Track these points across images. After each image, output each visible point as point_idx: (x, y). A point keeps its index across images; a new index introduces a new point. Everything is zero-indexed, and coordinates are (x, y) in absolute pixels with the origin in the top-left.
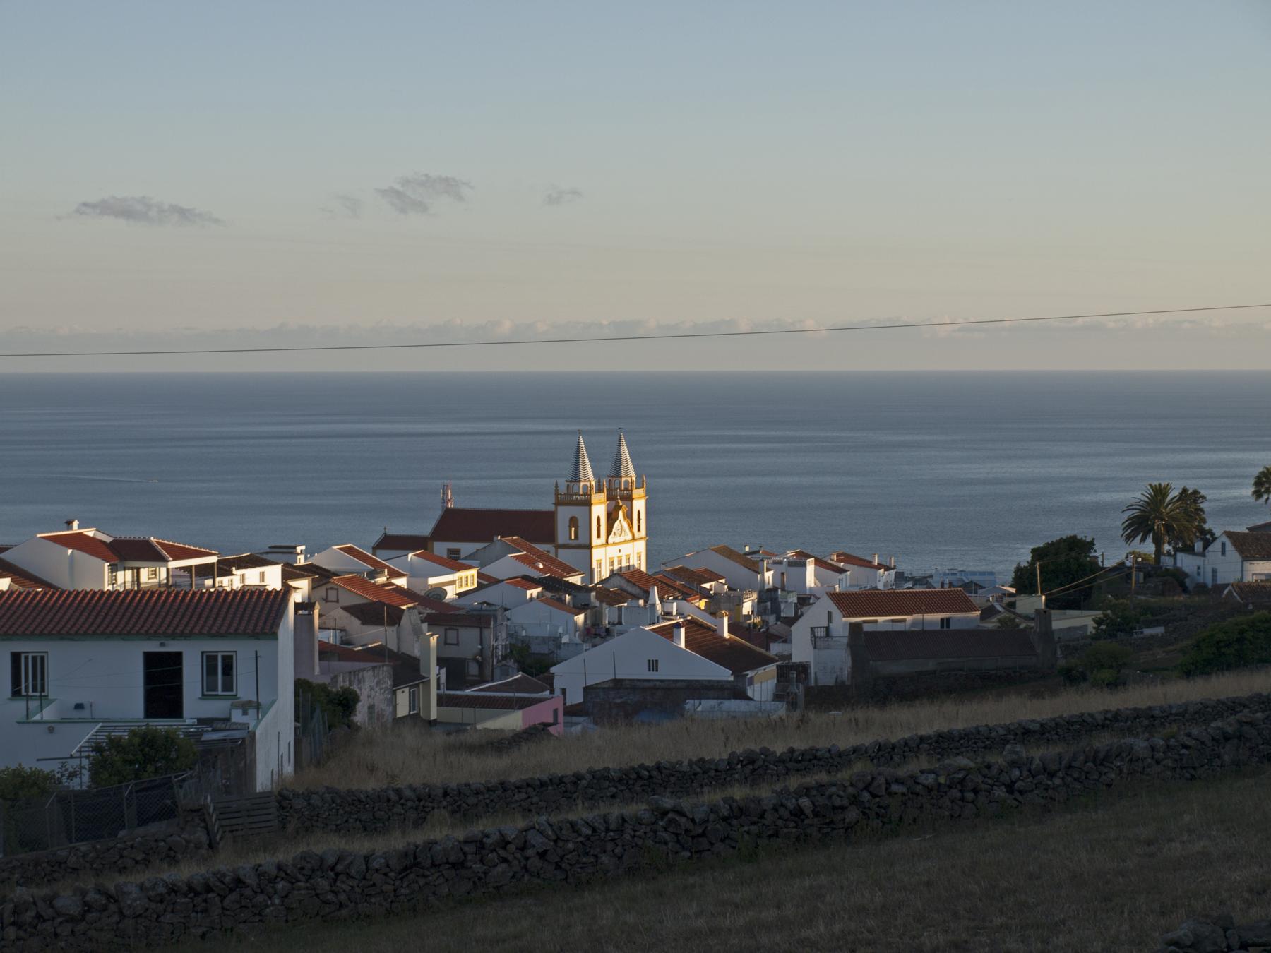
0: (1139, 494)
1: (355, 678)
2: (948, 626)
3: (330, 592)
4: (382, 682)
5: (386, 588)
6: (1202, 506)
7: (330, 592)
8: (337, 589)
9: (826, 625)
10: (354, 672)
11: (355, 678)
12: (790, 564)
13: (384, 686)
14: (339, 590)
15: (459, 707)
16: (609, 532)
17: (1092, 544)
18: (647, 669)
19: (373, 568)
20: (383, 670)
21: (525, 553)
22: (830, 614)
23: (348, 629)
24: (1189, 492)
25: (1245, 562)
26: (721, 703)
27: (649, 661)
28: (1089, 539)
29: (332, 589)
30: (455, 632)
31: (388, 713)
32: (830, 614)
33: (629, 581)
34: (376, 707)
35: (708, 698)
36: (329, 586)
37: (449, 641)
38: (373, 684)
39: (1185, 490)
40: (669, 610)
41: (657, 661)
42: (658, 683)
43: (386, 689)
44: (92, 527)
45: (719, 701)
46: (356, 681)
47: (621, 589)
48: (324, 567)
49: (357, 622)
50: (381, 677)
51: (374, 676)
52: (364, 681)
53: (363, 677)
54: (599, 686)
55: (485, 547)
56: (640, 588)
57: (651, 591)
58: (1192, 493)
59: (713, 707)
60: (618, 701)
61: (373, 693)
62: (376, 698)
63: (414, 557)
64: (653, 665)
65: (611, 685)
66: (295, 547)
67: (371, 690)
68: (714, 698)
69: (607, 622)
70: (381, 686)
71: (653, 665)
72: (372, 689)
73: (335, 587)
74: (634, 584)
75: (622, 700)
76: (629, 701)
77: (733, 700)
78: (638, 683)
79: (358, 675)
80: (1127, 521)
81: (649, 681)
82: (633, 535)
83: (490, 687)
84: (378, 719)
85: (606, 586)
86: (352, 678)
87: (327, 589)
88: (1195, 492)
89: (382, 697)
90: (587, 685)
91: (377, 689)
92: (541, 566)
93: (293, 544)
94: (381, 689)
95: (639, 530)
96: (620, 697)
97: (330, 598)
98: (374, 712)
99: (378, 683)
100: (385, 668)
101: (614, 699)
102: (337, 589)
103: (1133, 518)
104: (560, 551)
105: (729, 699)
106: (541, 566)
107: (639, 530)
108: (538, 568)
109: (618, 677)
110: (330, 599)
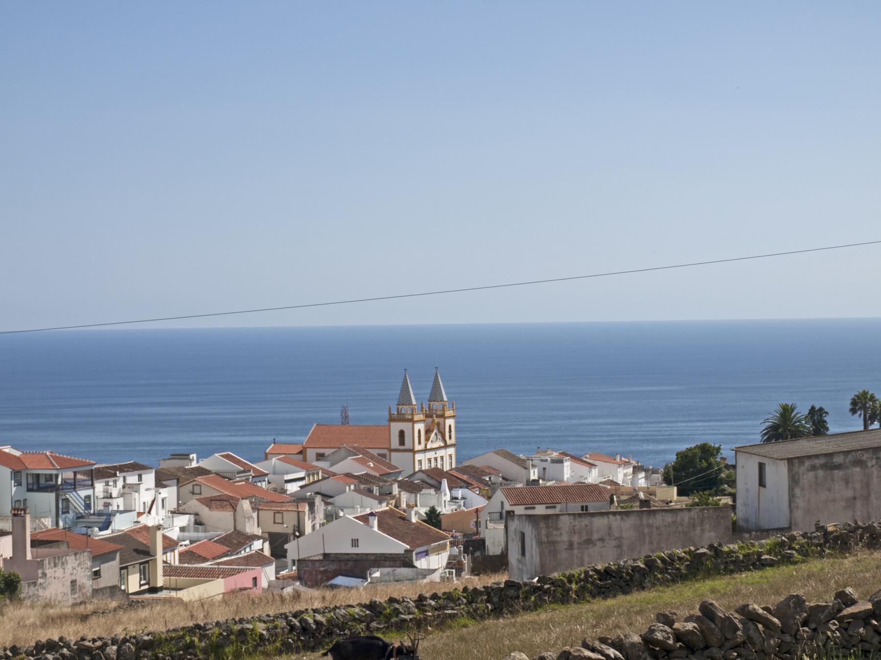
0: (773, 414)
1: (59, 561)
2: (587, 510)
3: (195, 487)
4: (83, 563)
5: (236, 484)
6: (825, 419)
7: (195, 487)
8: (200, 485)
9: (500, 511)
10: (58, 557)
11: (59, 561)
12: (554, 461)
13: (85, 566)
14: (202, 486)
15: (454, 555)
16: (427, 439)
17: (718, 449)
18: (351, 545)
19: (242, 469)
20: (84, 556)
21: (361, 456)
22: (502, 503)
23: (200, 513)
24: (816, 409)
25: (786, 462)
26: (394, 570)
27: (352, 540)
28: (717, 446)
29: (197, 485)
30: (281, 515)
31: (88, 585)
32: (502, 503)
33: (428, 476)
34: (77, 582)
35: (385, 567)
36: (194, 483)
37: (276, 521)
38: (75, 565)
39: (813, 408)
40: (456, 496)
41: (358, 540)
42: (354, 556)
43: (87, 568)
44: (7, 445)
45: (393, 569)
46: (60, 564)
47: (423, 481)
48: (207, 468)
49: (206, 509)
50: (82, 560)
51: (76, 559)
52: (67, 563)
53: (66, 560)
54: (311, 559)
55: (334, 453)
56: (436, 480)
57: (443, 482)
58: (818, 410)
59: (388, 574)
60: (322, 569)
61: (75, 571)
62: (77, 575)
63: (278, 462)
64: (355, 543)
65: (321, 558)
66: (189, 455)
67: (73, 569)
68: (389, 567)
69: (405, 505)
70: (82, 566)
71: (355, 543)
72: (74, 569)
73: (199, 484)
74: (432, 478)
75: (325, 568)
76: (330, 570)
77: (402, 568)
78: (340, 556)
79: (62, 559)
80: (766, 429)
81: (348, 554)
82: (445, 441)
83: (228, 561)
84: (80, 590)
85: (411, 479)
86: (57, 561)
87: (193, 486)
88: (821, 409)
89: (82, 574)
90: (300, 558)
91: (79, 569)
92: (372, 465)
93: (188, 453)
94: (82, 569)
95: (450, 438)
96: (323, 567)
97: (196, 492)
98: (76, 585)
99: (79, 564)
100: (85, 554)
101: (319, 568)
102: (200, 485)
103: (769, 428)
104: (393, 454)
105: (400, 567)
106: (372, 465)
107: (450, 438)
108: (369, 467)
109: (327, 552)
110: (195, 492)
